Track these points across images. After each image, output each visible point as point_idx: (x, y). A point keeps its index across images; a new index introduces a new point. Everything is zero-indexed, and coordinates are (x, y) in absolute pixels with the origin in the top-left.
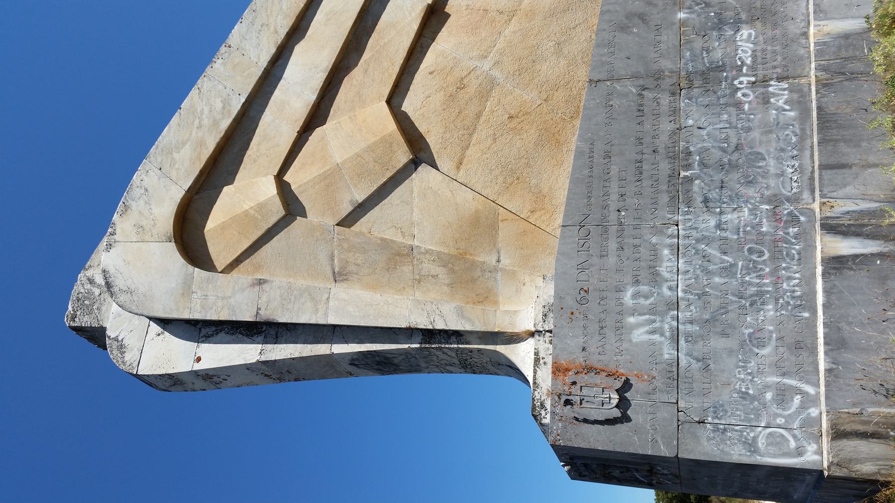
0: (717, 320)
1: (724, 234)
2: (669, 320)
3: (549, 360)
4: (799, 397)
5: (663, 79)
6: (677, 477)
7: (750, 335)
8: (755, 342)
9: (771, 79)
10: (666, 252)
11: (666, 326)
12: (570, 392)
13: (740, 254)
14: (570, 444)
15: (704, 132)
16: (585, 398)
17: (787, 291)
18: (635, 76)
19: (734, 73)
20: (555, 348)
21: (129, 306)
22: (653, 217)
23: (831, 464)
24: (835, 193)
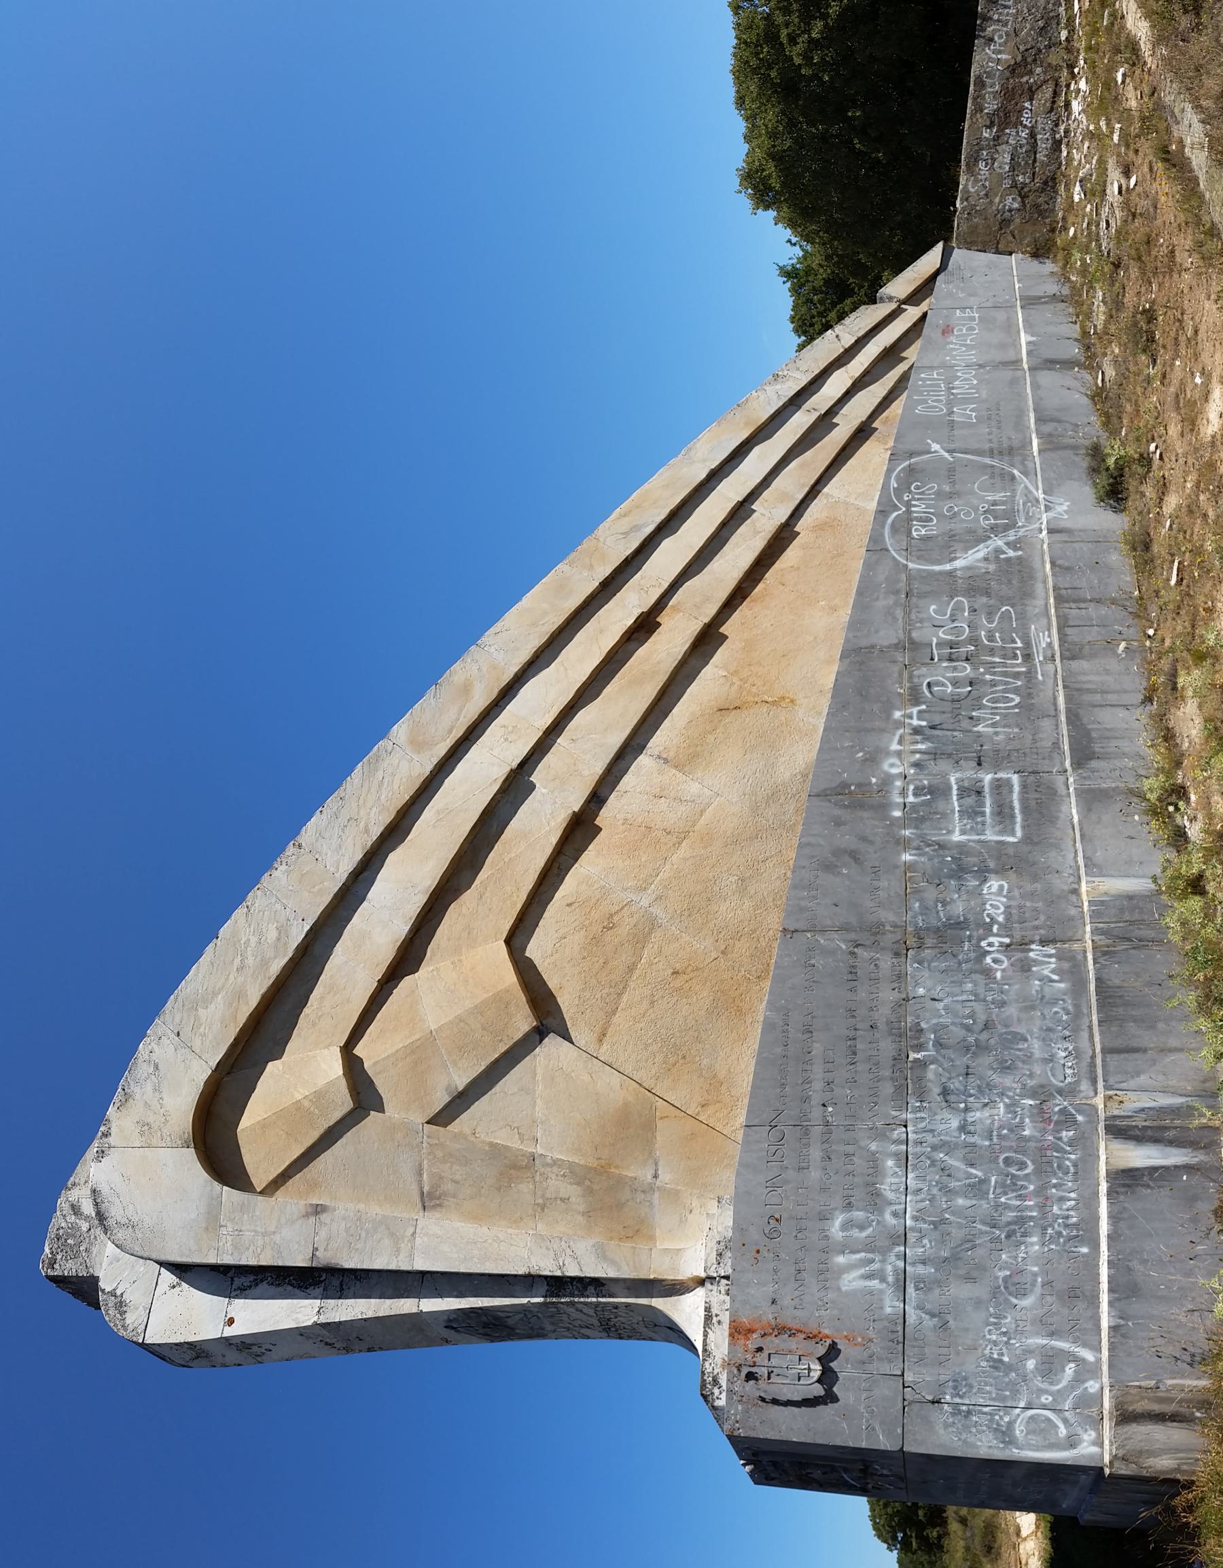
0: (960, 1258)
1: (971, 1139)
2: (893, 1258)
3: (726, 1318)
4: (1072, 1365)
5: (884, 934)
6: (902, 1479)
7: (1006, 1279)
8: (1012, 1289)
9: (1032, 942)
10: (890, 1163)
11: (889, 1268)
12: (754, 1362)
13: (993, 1166)
14: (753, 1434)
15: (940, 1005)
16: (774, 1370)
17: (1058, 1217)
18: (845, 928)
19: (981, 931)
20: (733, 1301)
21: (131, 1246)
22: (871, 1114)
23: (1114, 1458)
24: (1125, 1084)
